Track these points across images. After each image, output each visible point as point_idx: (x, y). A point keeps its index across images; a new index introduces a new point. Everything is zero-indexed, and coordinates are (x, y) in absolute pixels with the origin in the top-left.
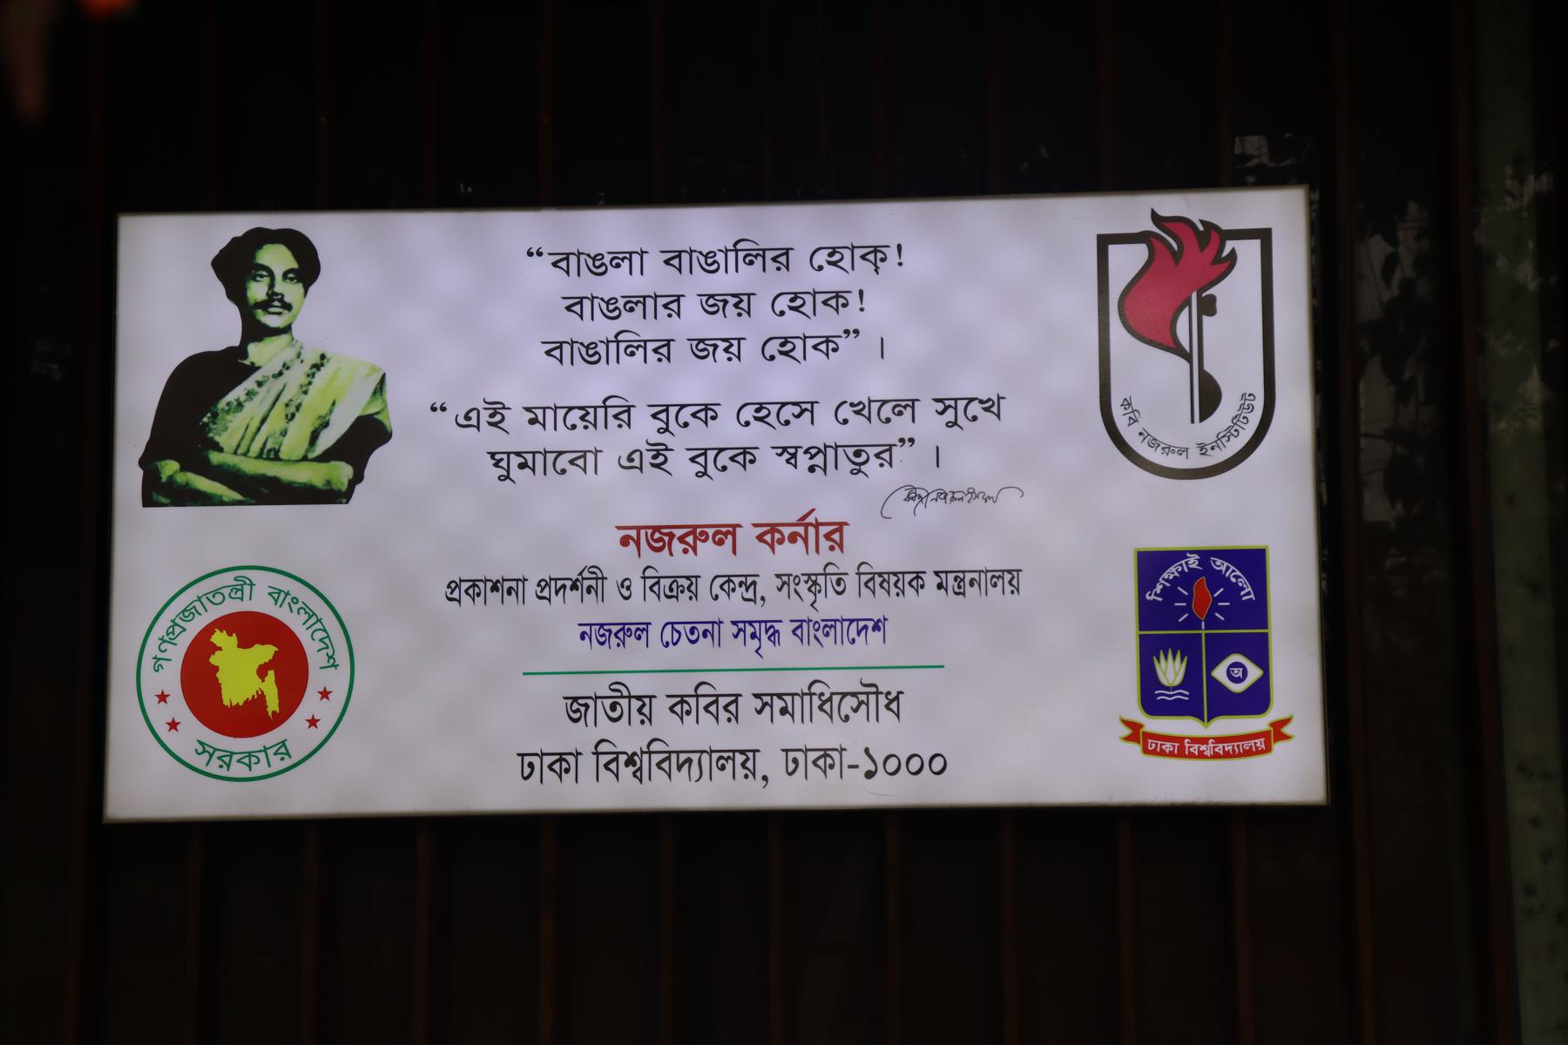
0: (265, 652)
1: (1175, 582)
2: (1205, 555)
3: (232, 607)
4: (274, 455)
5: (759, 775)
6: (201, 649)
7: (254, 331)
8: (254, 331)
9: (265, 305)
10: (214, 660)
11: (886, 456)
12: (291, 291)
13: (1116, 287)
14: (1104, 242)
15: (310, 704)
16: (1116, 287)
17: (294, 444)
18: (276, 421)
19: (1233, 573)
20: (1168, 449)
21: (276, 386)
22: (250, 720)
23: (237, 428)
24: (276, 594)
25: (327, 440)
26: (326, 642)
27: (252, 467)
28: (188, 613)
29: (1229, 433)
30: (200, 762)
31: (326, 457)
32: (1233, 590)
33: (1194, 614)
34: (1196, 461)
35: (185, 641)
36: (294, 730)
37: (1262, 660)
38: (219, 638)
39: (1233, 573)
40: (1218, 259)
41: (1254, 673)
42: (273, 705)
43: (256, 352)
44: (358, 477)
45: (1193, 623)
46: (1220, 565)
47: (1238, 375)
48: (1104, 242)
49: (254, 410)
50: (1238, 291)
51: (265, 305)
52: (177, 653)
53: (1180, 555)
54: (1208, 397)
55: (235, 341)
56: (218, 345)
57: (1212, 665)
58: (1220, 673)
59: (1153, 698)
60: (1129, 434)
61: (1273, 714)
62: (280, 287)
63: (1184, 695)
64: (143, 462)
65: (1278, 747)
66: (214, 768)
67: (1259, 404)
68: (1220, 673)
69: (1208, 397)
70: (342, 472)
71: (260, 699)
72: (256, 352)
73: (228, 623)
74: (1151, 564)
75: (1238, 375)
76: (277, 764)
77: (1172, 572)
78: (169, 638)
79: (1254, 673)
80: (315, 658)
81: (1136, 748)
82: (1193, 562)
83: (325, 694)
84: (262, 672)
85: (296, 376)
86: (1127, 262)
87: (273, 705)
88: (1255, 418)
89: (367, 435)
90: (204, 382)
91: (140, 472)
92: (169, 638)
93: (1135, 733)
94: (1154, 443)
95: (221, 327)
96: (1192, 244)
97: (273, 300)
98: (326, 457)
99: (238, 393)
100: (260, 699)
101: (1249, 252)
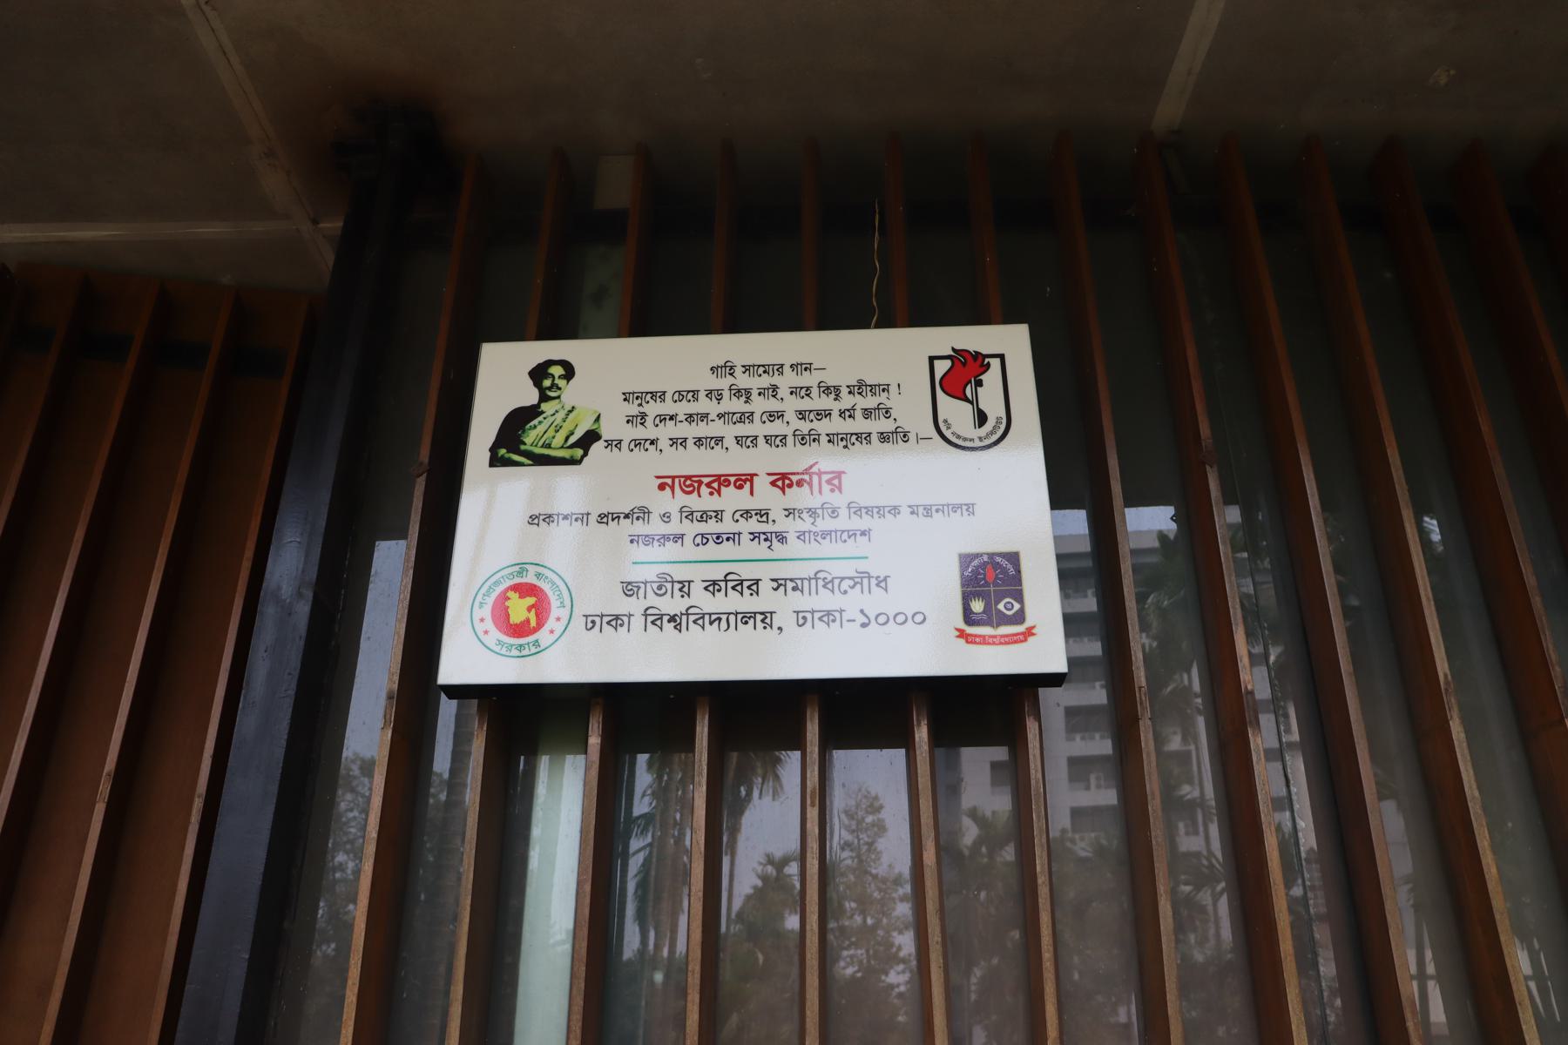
0: (531, 600)
1: (977, 567)
2: (992, 555)
3: (517, 580)
4: (549, 446)
5: (775, 626)
6: (503, 597)
7: (544, 398)
8: (544, 398)
9: (550, 388)
10: (508, 603)
11: (836, 482)
12: (562, 383)
13: (938, 377)
14: (932, 359)
15: (550, 623)
16: (938, 377)
17: (558, 440)
18: (551, 432)
19: (1004, 563)
20: (965, 439)
21: (551, 419)
22: (520, 630)
23: (531, 438)
24: (538, 575)
25: (572, 440)
26: (560, 596)
27: (538, 451)
28: (497, 583)
29: (992, 433)
30: (497, 649)
31: (572, 446)
32: (1004, 571)
33: (990, 584)
34: (978, 444)
35: (494, 595)
36: (543, 636)
37: (1019, 596)
38: (510, 594)
39: (1004, 563)
40: (982, 365)
41: (1017, 606)
42: (533, 623)
43: (544, 406)
44: (585, 454)
45: (987, 584)
46: (999, 559)
47: (994, 409)
48: (932, 359)
49: (541, 429)
50: (992, 378)
51: (550, 388)
52: (491, 600)
53: (977, 556)
54: (981, 418)
55: (535, 401)
56: (528, 404)
57: (997, 603)
58: (1001, 606)
59: (969, 617)
60: (948, 434)
61: (1028, 624)
62: (557, 381)
63: (985, 617)
64: (491, 450)
65: (1031, 639)
66: (504, 651)
67: (1004, 421)
68: (1001, 606)
69: (981, 418)
70: (579, 452)
71: (528, 621)
72: (544, 406)
73: (515, 588)
74: (966, 559)
75: (994, 409)
76: (534, 650)
77: (976, 563)
78: (487, 594)
79: (1017, 606)
80: (554, 603)
81: (962, 641)
82: (985, 558)
83: (558, 619)
84: (529, 609)
85: (561, 414)
86: (942, 367)
87: (533, 623)
88: (1003, 427)
89: (591, 438)
90: (518, 420)
91: (488, 454)
92: (487, 594)
93: (962, 634)
94: (959, 437)
95: (530, 396)
96: (970, 360)
97: (554, 386)
98: (572, 446)
99: (535, 422)
100: (528, 621)
101: (995, 363)
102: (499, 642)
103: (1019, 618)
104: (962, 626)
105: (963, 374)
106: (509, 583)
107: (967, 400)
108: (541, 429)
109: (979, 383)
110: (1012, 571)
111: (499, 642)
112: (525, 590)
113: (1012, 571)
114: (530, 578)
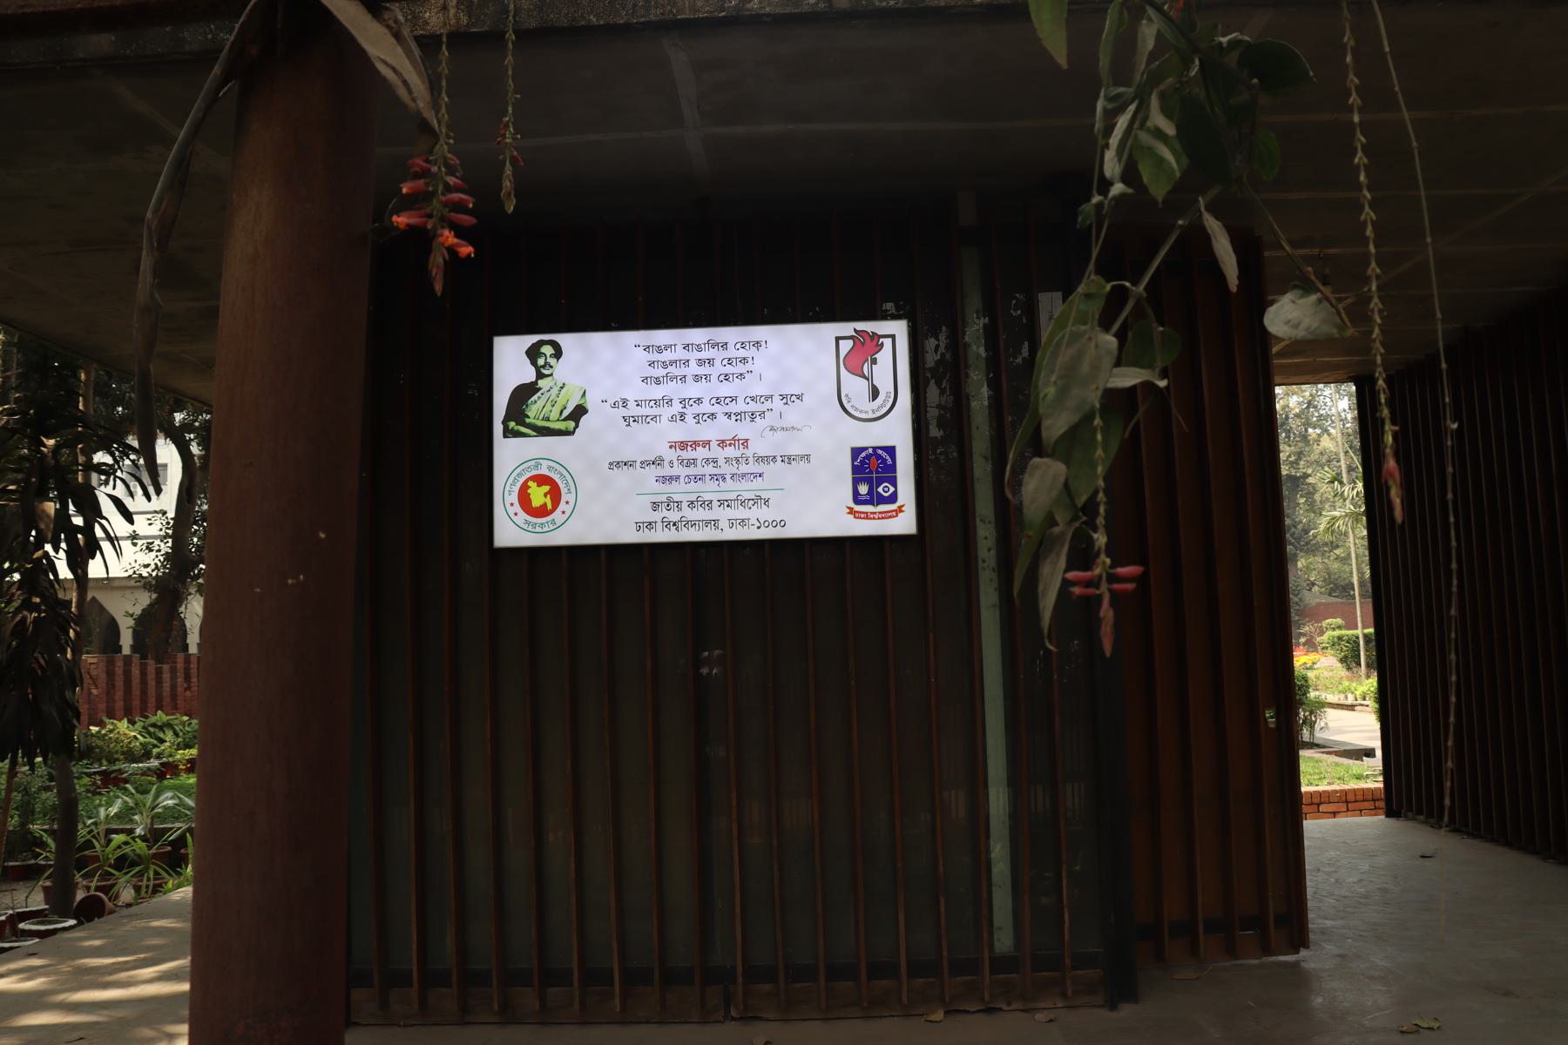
0: (546, 488)
3: (534, 473)
4: (548, 419)
6: (525, 487)
7: (540, 376)
8: (540, 376)
12: (552, 361)
14: (838, 339)
17: (554, 415)
22: (542, 512)
24: (550, 468)
25: (566, 413)
27: (541, 423)
28: (519, 475)
35: (519, 485)
36: (557, 516)
41: (892, 489)
42: (549, 506)
47: (885, 386)
48: (838, 339)
49: (540, 403)
50: (885, 356)
52: (516, 489)
54: (875, 393)
58: (880, 490)
59: (857, 499)
68: (880, 490)
69: (875, 393)
70: (571, 424)
71: (545, 505)
73: (533, 478)
74: (856, 452)
75: (885, 386)
79: (892, 489)
85: (555, 391)
86: (846, 346)
87: (549, 506)
90: (523, 394)
93: (851, 512)
95: (529, 375)
97: (546, 365)
100: (545, 505)
101: (888, 342)
102: (526, 522)
103: (893, 498)
104: (852, 505)
105: (867, 347)
106: (529, 475)
107: (864, 376)
108: (540, 403)
109: (874, 362)
110: (889, 461)
111: (526, 522)
112: (541, 480)
113: (889, 461)
114: (544, 471)
